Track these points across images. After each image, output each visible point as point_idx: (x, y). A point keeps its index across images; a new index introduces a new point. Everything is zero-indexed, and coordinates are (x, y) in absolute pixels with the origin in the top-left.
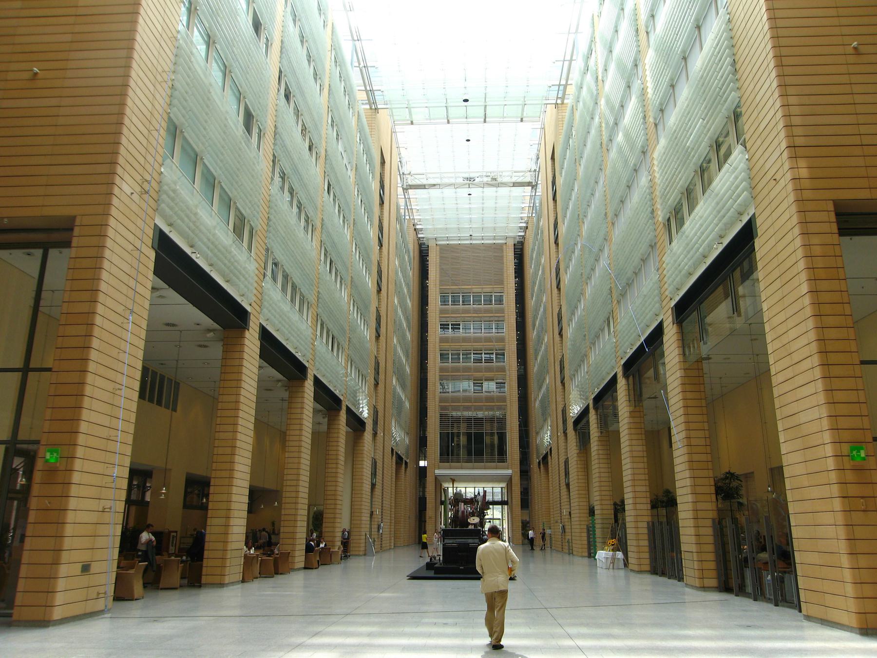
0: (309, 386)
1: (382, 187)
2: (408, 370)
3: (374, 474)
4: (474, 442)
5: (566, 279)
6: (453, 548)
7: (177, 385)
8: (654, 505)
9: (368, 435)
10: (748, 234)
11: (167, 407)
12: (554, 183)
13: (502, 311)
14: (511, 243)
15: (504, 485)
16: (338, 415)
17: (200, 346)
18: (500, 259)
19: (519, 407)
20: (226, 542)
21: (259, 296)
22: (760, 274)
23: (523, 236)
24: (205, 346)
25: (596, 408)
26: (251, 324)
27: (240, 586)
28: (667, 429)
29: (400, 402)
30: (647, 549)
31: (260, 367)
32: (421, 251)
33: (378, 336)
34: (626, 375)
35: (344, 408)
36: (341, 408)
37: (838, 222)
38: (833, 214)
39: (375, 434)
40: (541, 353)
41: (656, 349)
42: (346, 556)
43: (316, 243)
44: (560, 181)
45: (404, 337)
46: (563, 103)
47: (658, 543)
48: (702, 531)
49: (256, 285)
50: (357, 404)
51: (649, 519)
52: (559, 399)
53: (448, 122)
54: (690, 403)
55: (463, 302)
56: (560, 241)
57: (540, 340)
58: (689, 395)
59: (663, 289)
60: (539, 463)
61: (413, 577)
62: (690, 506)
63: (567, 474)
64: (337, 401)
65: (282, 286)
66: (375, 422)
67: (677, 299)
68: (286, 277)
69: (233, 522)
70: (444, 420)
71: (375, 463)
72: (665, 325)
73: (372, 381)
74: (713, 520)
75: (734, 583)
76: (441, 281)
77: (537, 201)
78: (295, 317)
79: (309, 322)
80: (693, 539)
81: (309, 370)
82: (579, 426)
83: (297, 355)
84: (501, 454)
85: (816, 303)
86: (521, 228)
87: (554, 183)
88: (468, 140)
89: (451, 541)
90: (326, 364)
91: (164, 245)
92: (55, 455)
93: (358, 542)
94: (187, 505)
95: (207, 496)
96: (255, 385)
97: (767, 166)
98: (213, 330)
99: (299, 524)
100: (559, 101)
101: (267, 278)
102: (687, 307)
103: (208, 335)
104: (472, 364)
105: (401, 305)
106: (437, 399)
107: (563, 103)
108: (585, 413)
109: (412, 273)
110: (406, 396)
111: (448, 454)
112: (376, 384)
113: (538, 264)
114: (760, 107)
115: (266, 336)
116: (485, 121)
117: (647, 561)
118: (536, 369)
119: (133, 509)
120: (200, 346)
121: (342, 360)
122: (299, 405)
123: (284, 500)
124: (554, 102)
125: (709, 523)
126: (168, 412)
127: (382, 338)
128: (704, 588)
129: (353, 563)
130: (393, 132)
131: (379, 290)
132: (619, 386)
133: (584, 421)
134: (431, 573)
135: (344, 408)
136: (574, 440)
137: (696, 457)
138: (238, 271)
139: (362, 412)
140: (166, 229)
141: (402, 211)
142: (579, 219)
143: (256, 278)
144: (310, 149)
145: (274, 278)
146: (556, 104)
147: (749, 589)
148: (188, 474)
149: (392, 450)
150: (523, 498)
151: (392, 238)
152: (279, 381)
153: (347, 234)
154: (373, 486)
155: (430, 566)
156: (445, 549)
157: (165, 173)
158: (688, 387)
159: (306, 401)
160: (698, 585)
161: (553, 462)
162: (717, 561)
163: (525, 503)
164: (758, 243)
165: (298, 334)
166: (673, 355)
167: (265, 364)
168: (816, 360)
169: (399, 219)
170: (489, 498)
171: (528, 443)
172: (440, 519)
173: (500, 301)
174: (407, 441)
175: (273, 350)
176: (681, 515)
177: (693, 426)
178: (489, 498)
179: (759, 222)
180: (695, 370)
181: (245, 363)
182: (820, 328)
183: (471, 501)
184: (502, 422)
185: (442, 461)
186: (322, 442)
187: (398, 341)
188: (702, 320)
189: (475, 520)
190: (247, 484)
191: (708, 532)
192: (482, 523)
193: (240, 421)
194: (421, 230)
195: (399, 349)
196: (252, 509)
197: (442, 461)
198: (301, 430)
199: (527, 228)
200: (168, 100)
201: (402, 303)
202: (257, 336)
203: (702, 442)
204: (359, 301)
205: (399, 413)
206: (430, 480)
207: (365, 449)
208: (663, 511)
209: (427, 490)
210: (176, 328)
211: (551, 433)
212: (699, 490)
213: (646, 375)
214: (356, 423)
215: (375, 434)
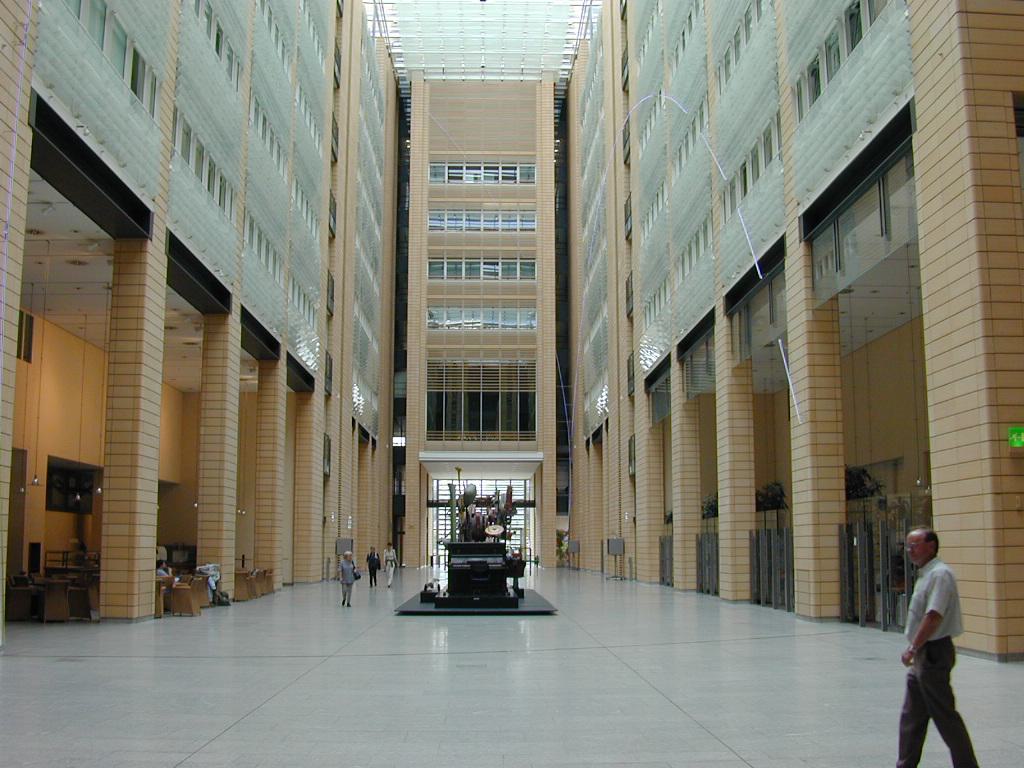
2: (376, 289)
3: (327, 457)
4: (482, 406)
5: (638, 153)
8: (761, 506)
13: (532, 195)
15: (530, 476)
16: (274, 367)
17: (74, 262)
18: (531, 106)
20: (131, 559)
21: (165, 184)
29: (365, 343)
32: (398, 91)
36: (278, 354)
39: (328, 396)
40: (595, 267)
41: (773, 277)
43: (244, 92)
45: (370, 235)
51: (752, 526)
52: (624, 342)
56: (631, 87)
57: (595, 245)
59: (788, 188)
60: (588, 442)
62: (810, 508)
63: (632, 459)
64: (274, 345)
65: (196, 169)
66: (329, 377)
67: (807, 205)
68: (200, 151)
70: (435, 372)
72: (788, 242)
73: (325, 312)
75: (860, 613)
78: (213, 214)
80: (810, 553)
82: (653, 388)
83: (216, 275)
84: (526, 424)
85: (983, 235)
89: (460, 561)
90: (257, 287)
91: (45, 119)
97: (933, 32)
99: (225, 535)
102: (819, 217)
104: (481, 282)
106: (424, 339)
108: (664, 366)
110: (373, 333)
111: (438, 424)
112: (330, 316)
113: (595, 121)
115: (176, 249)
117: (747, 586)
120: (74, 262)
121: (281, 280)
125: (834, 530)
127: (338, 240)
128: (821, 619)
131: (334, 161)
132: (717, 328)
133: (661, 381)
134: (431, 607)
136: (646, 409)
138: (133, 146)
140: (45, 95)
141: (370, 25)
143: (162, 158)
145: (186, 154)
147: (879, 617)
148: (50, 459)
153: (289, 73)
154: (326, 477)
156: (453, 573)
157: (44, 10)
159: (230, 347)
161: (609, 440)
162: (842, 582)
164: (917, 139)
168: (978, 312)
169: (365, 40)
170: (518, 496)
171: (569, 409)
173: (528, 175)
174: (375, 406)
176: (797, 520)
179: (919, 110)
180: (827, 315)
182: (986, 269)
183: (487, 502)
184: (528, 374)
187: (363, 244)
189: (494, 530)
191: (832, 542)
194: (400, 55)
195: (363, 256)
198: (224, 392)
201: (369, 180)
204: (305, 186)
205: (363, 361)
206: (411, 467)
207: (315, 420)
208: (772, 515)
210: (39, 237)
211: (610, 390)
213: (757, 314)
215: (328, 396)
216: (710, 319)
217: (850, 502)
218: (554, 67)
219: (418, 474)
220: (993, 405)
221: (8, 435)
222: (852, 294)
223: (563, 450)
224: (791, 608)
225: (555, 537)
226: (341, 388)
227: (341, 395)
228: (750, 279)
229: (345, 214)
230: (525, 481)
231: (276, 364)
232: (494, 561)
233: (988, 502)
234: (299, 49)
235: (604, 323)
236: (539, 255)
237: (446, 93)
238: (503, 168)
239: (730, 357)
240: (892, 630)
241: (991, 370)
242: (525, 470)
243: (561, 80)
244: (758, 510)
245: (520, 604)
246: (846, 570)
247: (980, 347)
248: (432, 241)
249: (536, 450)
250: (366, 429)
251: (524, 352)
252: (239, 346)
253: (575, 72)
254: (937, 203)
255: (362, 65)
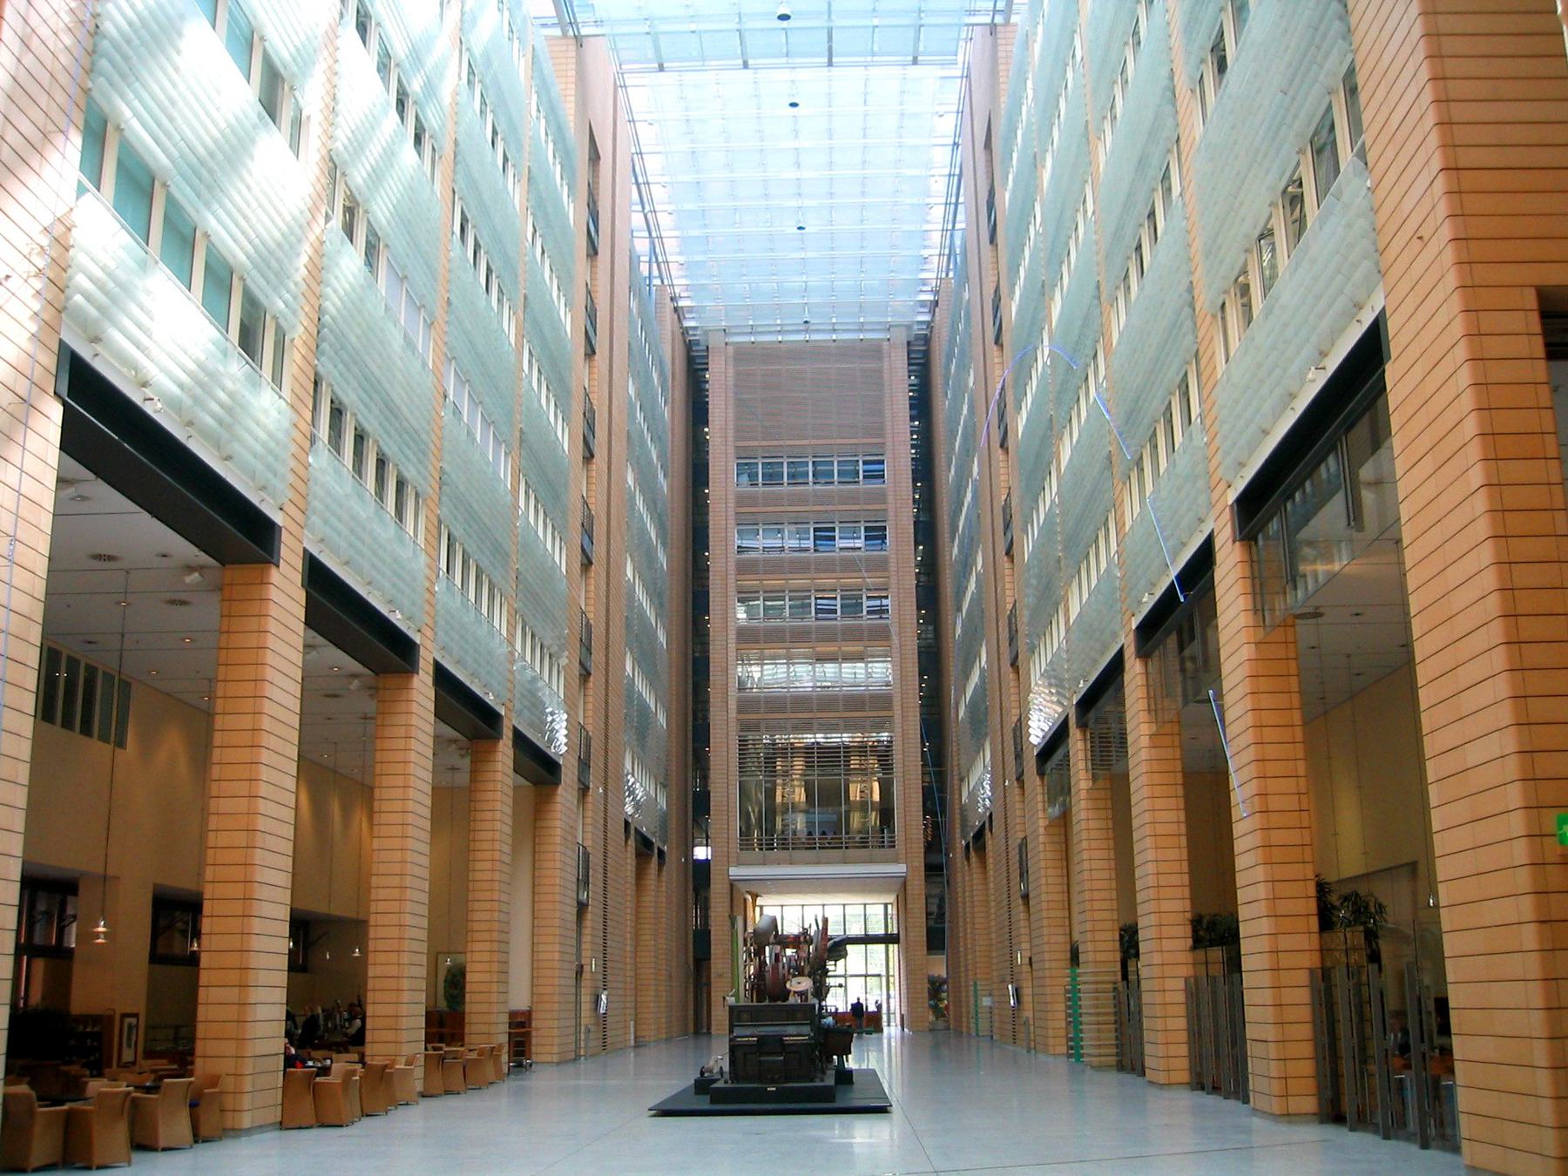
0: (422, 687)
1: (594, 215)
2: (662, 638)
6: (749, 1045)
7: (126, 686)
9: (566, 793)
10: (1371, 352)
11: (104, 738)
12: (991, 205)
13: (881, 497)
14: (901, 337)
15: (891, 898)
16: (493, 750)
17: (173, 602)
18: (876, 379)
19: (923, 720)
20: (241, 1040)
22: (1397, 442)
23: (928, 324)
24: (183, 603)
25: (1082, 725)
26: (284, 551)
27: (277, 1134)
31: (308, 647)
33: (587, 563)
34: (1144, 653)
35: (507, 734)
37: (1546, 333)
38: (1535, 318)
39: (584, 790)
42: (520, 1065)
44: (1005, 198)
47: (1207, 1024)
48: (1288, 996)
49: (293, 463)
50: (541, 724)
51: (1186, 971)
53: (746, 65)
54: (1268, 718)
55: (792, 476)
56: (1006, 338)
57: (966, 564)
58: (1266, 701)
59: (1214, 462)
60: (967, 846)
61: (664, 1112)
66: (584, 765)
67: (1240, 485)
69: (255, 995)
71: (586, 855)
72: (1218, 543)
74: (1312, 971)
75: (1348, 1106)
76: (738, 430)
77: (958, 242)
79: (421, 540)
80: (1269, 1014)
81: (422, 652)
86: (923, 304)
87: (991, 205)
88: (794, 105)
93: (548, 1036)
94: (156, 957)
95: (197, 934)
96: (296, 690)
98: (200, 568)
100: (999, 19)
101: (319, 444)
102: (1256, 504)
103: (188, 579)
105: (641, 494)
107: (1007, 22)
108: (1059, 736)
109: (670, 411)
111: (764, 832)
113: (961, 388)
114: (1392, 74)
115: (318, 577)
116: (830, 64)
118: (959, 631)
119: (40, 965)
120: (173, 602)
122: (401, 731)
123: (372, 945)
124: (988, 20)
125: (1303, 977)
126: (107, 748)
128: (1289, 1117)
129: (542, 1080)
130: (619, 86)
131: (589, 457)
132: (1127, 677)
133: (1058, 756)
134: (704, 1103)
135: (507, 734)
137: (1277, 837)
138: (250, 427)
139: (551, 740)
140: (85, 352)
141: (644, 269)
142: (1041, 293)
144: (418, 140)
146: (993, 28)
149: (627, 824)
150: (933, 929)
151: (621, 330)
152: (355, 676)
155: (703, 1085)
158: (1264, 684)
160: (1276, 1110)
162: (1318, 1059)
163: (936, 940)
164: (1391, 372)
165: (395, 568)
166: (1231, 613)
167: (320, 640)
168: (1496, 632)
172: (732, 982)
174: (662, 803)
175: (334, 606)
177: (1271, 768)
178: (834, 930)
179: (1392, 326)
181: (271, 642)
183: (797, 941)
186: (454, 807)
188: (1291, 533)
189: (805, 984)
190: (284, 913)
192: (821, 991)
193: (265, 773)
196: (298, 964)
200: (86, 61)
202: (298, 579)
203: (1290, 803)
206: (718, 889)
208: (1216, 954)
209: (712, 914)
212: (1284, 907)
214: (538, 767)
215: (584, 790)
216: (1116, 667)
217: (1325, 935)
218: (906, 320)
219: (728, 900)
220: (1529, 779)
222: (1320, 620)
223: (935, 859)
224: (1246, 1101)
225: (927, 986)
226: (606, 778)
227: (606, 790)
228: (1167, 602)
229: (608, 533)
230: (886, 905)
231: (496, 745)
232: (796, 1034)
233: (1529, 937)
234: (525, 297)
235: (982, 676)
237: (765, 362)
240: (1397, 1138)
241: (1523, 724)
242: (888, 891)
243: (918, 337)
244: (1195, 947)
245: (838, 1097)
246: (1326, 1039)
247: (1501, 687)
249: (896, 861)
250: (649, 836)
252: (431, 718)
253: (936, 325)
254: (1427, 466)
255: (631, 322)
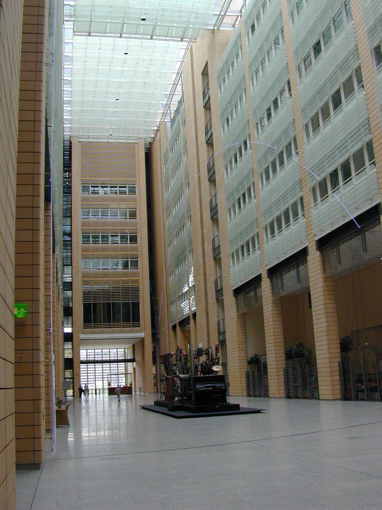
18: (133, 155)
28: (307, 295)
30: (338, 382)
46: (218, 29)
76: (82, 173)
92: (23, 310)
106: (80, 275)
125: (337, 364)
184: (136, 290)
185: (85, 327)
197: (85, 327)
199: (158, 130)
221: (298, 273)
230: (125, 349)
236: (139, 231)
237: (90, 148)
238: (120, 187)
239: (322, 272)
248: (83, 224)
249: (141, 332)
251: (133, 281)
